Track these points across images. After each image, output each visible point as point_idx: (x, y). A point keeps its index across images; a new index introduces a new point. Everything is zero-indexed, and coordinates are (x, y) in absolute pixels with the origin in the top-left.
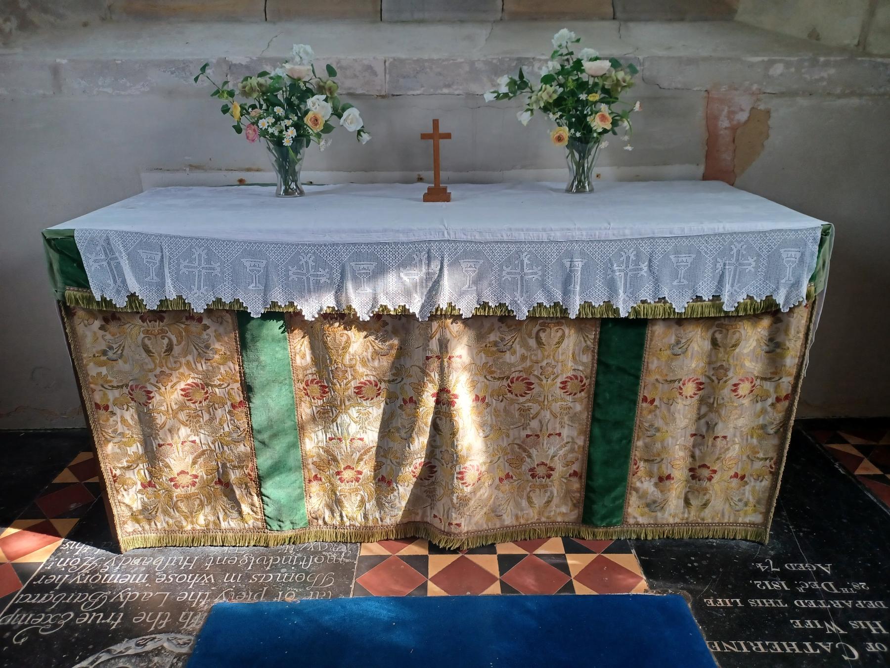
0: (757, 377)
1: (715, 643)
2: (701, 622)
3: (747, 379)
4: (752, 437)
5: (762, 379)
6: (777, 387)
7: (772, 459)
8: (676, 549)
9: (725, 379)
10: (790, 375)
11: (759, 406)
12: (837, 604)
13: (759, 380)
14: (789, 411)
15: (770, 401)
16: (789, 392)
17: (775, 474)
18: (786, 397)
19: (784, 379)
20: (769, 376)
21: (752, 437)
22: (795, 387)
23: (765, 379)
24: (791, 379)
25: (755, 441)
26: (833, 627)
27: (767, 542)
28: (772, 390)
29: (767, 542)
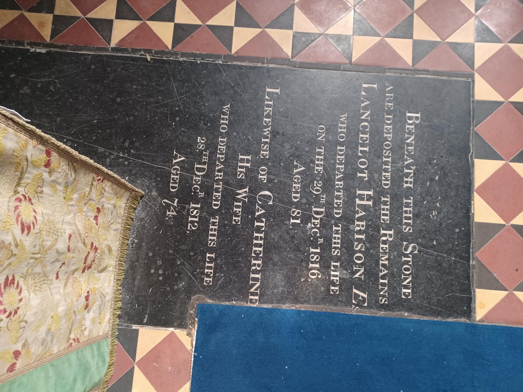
0: (16, 192)
1: (251, 297)
2: (229, 299)
3: (17, 208)
4: (71, 199)
5: (18, 185)
6: (35, 166)
7: (94, 178)
8: (136, 283)
9: (13, 247)
10: (27, 144)
11: (46, 190)
12: (219, 176)
13: (20, 189)
14: (63, 153)
15: (46, 176)
16: (44, 148)
17: (107, 177)
18: (48, 154)
19: (29, 155)
20: (18, 173)
21: (71, 199)
22: (42, 141)
23: (20, 179)
24: (32, 143)
25: (75, 196)
26: (243, 193)
27: (143, 193)
28: (35, 172)
29: (143, 193)
